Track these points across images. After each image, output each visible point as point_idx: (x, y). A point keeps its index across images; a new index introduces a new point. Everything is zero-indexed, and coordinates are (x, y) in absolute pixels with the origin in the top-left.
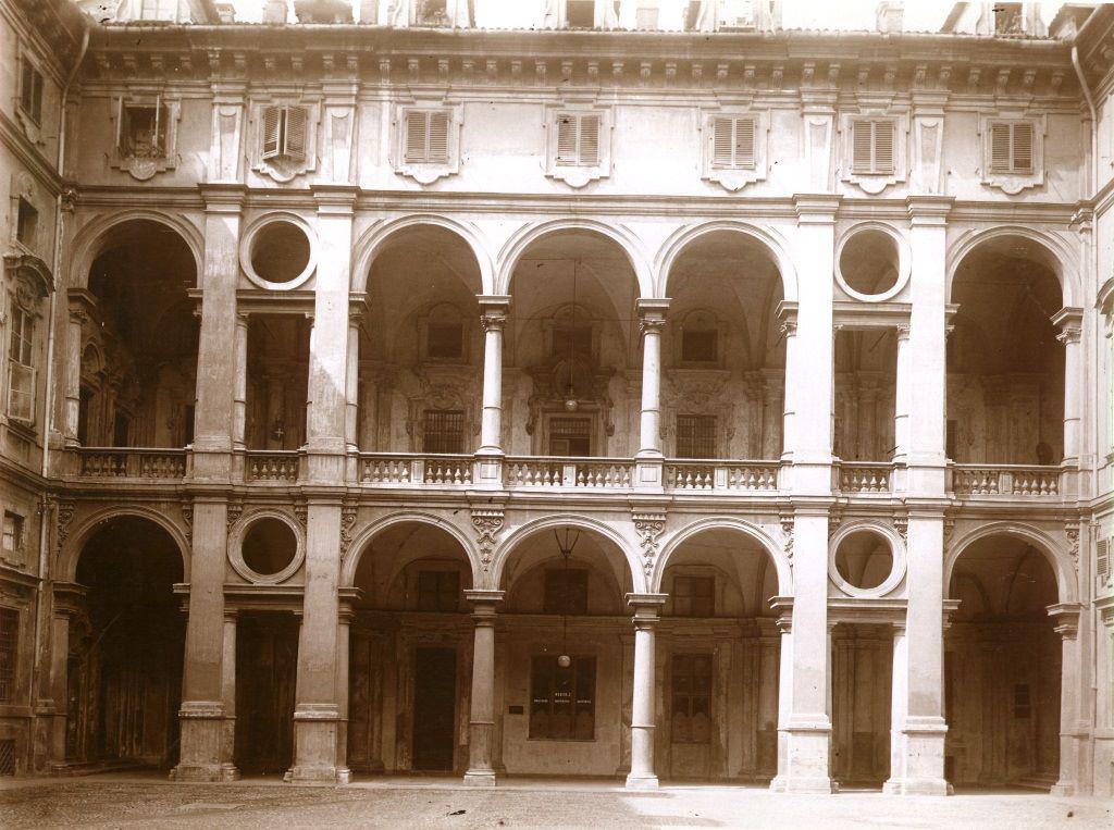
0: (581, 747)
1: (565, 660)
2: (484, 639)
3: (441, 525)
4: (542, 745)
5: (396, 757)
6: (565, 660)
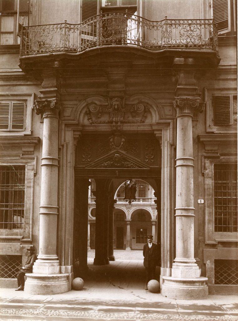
1: (142, 230)
2: (128, 227)
4: (138, 244)
5: (184, 282)
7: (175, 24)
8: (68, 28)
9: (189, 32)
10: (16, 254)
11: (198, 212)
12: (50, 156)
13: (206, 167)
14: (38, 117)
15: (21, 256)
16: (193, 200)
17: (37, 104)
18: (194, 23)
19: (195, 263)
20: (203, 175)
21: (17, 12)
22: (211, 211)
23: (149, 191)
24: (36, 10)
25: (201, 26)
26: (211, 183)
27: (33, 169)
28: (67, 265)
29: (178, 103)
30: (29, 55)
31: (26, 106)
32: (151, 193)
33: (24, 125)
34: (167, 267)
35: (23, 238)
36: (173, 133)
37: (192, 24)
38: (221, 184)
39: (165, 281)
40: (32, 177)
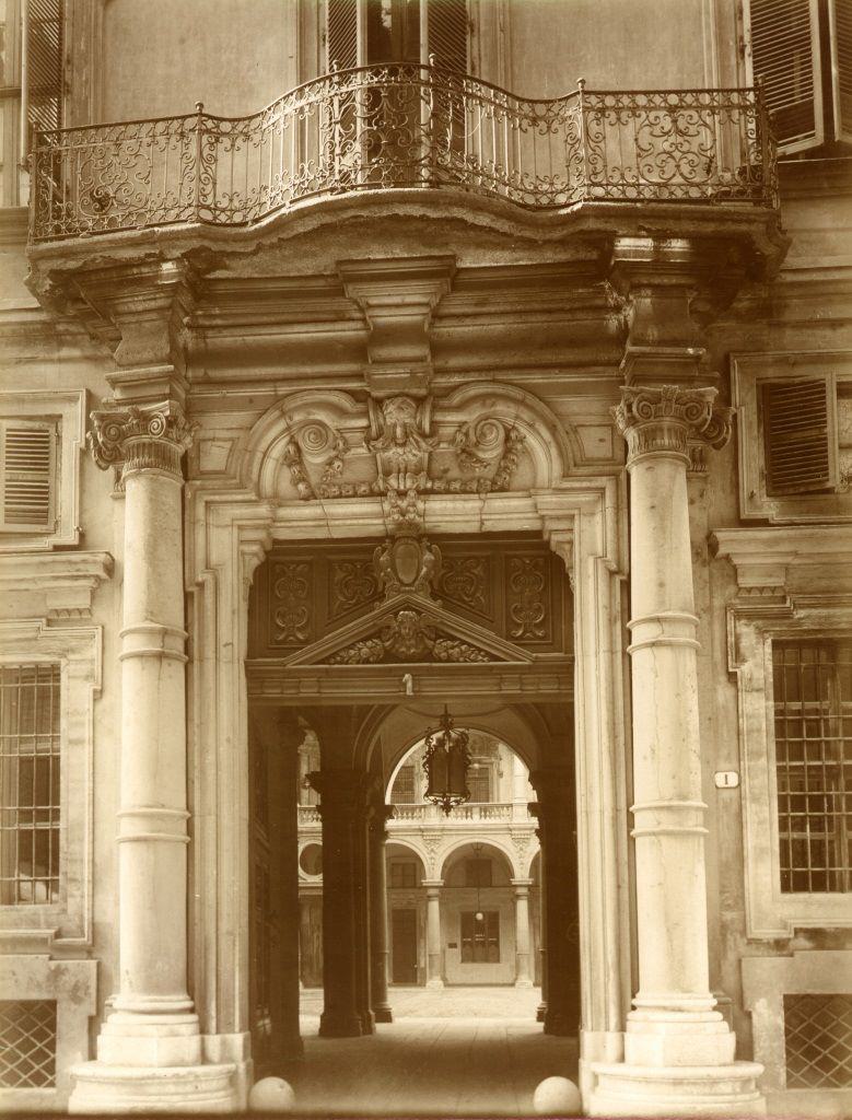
0: (493, 967)
1: (480, 916)
2: (434, 906)
3: (405, 843)
4: (469, 966)
6: (480, 916)
7: (618, 110)
8: (208, 131)
9: (672, 139)
10: (35, 995)
11: (718, 820)
12: (152, 621)
13: (742, 651)
14: (102, 478)
15: (52, 1004)
16: (699, 774)
17: (100, 427)
18: (689, 103)
19: (715, 1009)
20: (732, 678)
21: (20, 90)
22: (767, 815)
23: (501, 780)
24: (87, 79)
25: (713, 113)
26: (763, 711)
27: (89, 677)
28: (229, 1032)
29: (634, 409)
30: (62, 239)
31: (59, 437)
32: (514, 781)
33: (52, 510)
34: (607, 1029)
35: (58, 935)
36: (617, 522)
37: (682, 107)
38: (799, 712)
39: (601, 1079)
40: (88, 704)
